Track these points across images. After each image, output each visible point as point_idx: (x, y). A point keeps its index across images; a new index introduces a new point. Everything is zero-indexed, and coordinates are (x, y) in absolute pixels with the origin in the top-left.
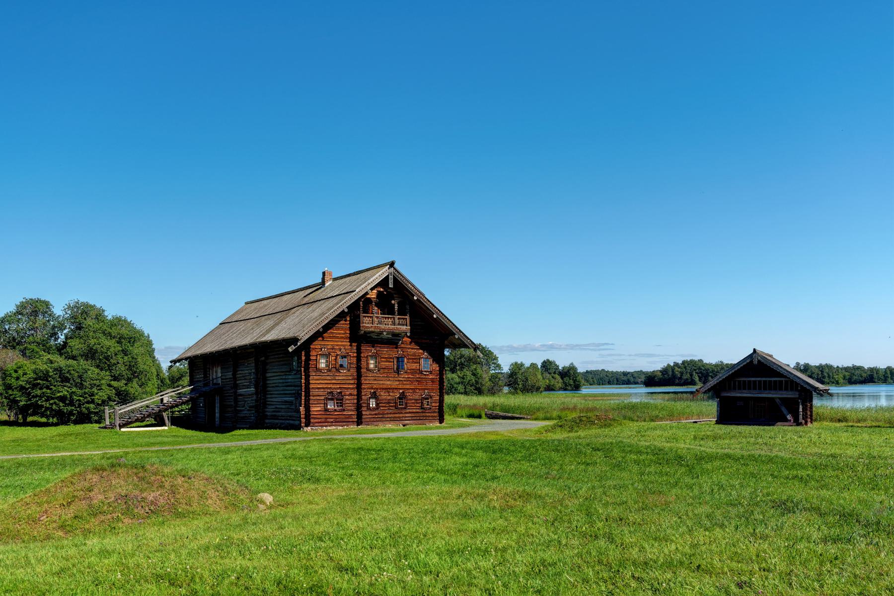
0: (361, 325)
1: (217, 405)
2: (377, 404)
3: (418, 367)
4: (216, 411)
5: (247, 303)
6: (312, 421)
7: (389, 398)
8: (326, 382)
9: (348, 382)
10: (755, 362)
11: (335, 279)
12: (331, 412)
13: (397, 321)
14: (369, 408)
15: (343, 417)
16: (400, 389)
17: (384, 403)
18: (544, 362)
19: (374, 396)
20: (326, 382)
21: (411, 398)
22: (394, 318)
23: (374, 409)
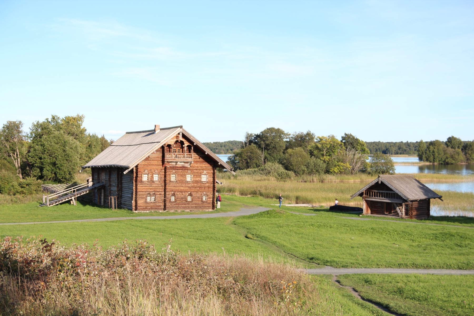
0: (165, 159)
1: (103, 194)
2: (175, 199)
3: (200, 180)
4: (102, 198)
5: (127, 133)
6: (138, 208)
7: (182, 196)
8: (146, 188)
9: (159, 188)
10: (380, 183)
11: (161, 129)
12: (149, 203)
13: (186, 156)
14: (170, 201)
15: (155, 206)
16: (189, 191)
17: (180, 199)
18: (450, 138)
19: (174, 195)
20: (146, 188)
21: (195, 196)
22: (184, 154)
23: (174, 202)
